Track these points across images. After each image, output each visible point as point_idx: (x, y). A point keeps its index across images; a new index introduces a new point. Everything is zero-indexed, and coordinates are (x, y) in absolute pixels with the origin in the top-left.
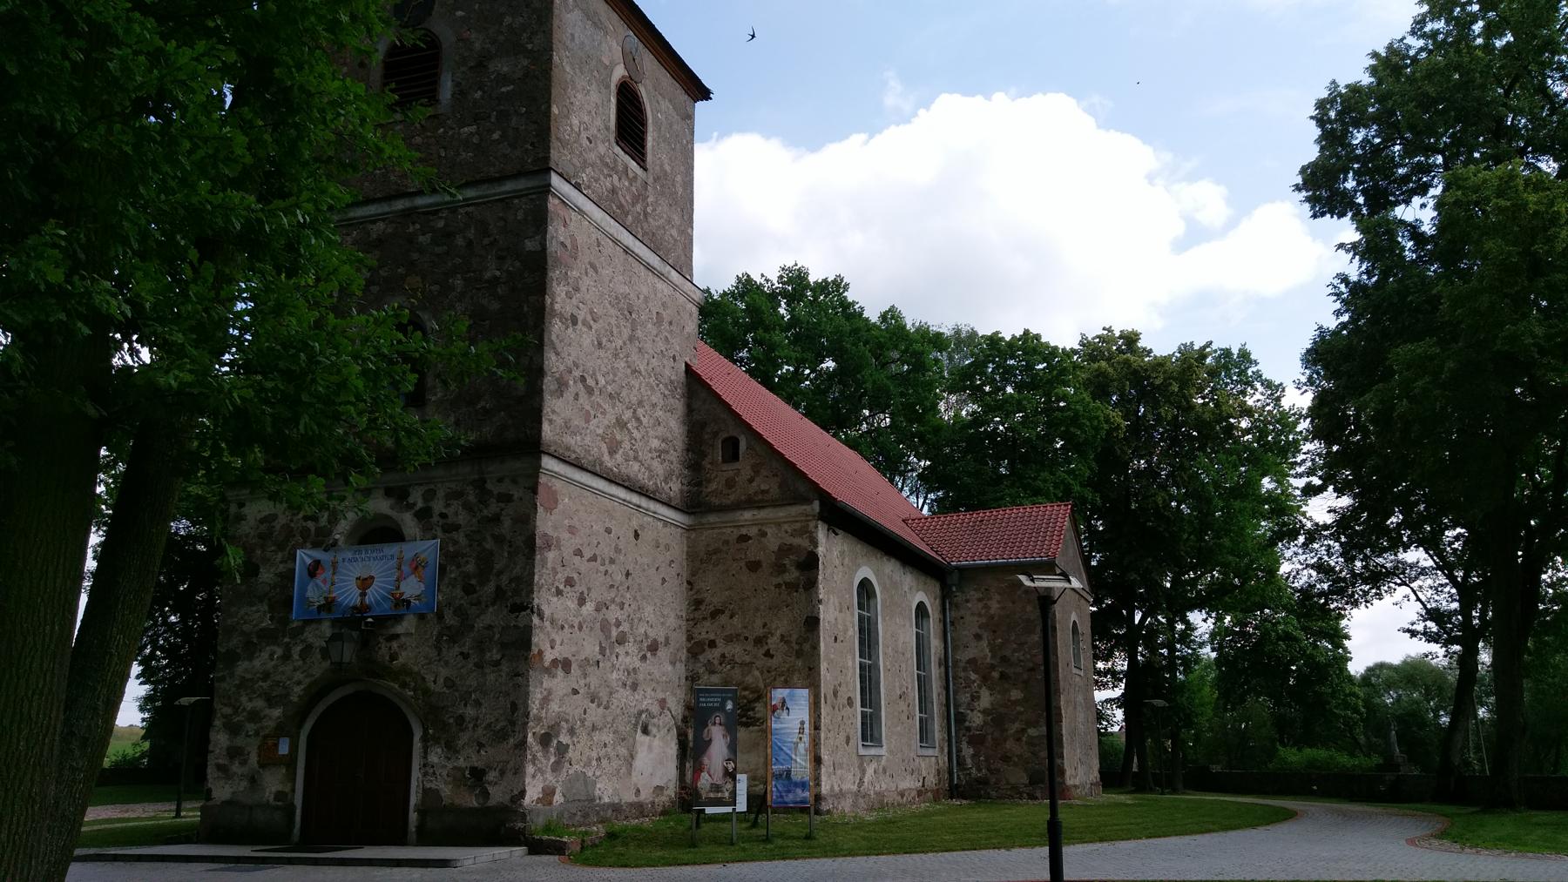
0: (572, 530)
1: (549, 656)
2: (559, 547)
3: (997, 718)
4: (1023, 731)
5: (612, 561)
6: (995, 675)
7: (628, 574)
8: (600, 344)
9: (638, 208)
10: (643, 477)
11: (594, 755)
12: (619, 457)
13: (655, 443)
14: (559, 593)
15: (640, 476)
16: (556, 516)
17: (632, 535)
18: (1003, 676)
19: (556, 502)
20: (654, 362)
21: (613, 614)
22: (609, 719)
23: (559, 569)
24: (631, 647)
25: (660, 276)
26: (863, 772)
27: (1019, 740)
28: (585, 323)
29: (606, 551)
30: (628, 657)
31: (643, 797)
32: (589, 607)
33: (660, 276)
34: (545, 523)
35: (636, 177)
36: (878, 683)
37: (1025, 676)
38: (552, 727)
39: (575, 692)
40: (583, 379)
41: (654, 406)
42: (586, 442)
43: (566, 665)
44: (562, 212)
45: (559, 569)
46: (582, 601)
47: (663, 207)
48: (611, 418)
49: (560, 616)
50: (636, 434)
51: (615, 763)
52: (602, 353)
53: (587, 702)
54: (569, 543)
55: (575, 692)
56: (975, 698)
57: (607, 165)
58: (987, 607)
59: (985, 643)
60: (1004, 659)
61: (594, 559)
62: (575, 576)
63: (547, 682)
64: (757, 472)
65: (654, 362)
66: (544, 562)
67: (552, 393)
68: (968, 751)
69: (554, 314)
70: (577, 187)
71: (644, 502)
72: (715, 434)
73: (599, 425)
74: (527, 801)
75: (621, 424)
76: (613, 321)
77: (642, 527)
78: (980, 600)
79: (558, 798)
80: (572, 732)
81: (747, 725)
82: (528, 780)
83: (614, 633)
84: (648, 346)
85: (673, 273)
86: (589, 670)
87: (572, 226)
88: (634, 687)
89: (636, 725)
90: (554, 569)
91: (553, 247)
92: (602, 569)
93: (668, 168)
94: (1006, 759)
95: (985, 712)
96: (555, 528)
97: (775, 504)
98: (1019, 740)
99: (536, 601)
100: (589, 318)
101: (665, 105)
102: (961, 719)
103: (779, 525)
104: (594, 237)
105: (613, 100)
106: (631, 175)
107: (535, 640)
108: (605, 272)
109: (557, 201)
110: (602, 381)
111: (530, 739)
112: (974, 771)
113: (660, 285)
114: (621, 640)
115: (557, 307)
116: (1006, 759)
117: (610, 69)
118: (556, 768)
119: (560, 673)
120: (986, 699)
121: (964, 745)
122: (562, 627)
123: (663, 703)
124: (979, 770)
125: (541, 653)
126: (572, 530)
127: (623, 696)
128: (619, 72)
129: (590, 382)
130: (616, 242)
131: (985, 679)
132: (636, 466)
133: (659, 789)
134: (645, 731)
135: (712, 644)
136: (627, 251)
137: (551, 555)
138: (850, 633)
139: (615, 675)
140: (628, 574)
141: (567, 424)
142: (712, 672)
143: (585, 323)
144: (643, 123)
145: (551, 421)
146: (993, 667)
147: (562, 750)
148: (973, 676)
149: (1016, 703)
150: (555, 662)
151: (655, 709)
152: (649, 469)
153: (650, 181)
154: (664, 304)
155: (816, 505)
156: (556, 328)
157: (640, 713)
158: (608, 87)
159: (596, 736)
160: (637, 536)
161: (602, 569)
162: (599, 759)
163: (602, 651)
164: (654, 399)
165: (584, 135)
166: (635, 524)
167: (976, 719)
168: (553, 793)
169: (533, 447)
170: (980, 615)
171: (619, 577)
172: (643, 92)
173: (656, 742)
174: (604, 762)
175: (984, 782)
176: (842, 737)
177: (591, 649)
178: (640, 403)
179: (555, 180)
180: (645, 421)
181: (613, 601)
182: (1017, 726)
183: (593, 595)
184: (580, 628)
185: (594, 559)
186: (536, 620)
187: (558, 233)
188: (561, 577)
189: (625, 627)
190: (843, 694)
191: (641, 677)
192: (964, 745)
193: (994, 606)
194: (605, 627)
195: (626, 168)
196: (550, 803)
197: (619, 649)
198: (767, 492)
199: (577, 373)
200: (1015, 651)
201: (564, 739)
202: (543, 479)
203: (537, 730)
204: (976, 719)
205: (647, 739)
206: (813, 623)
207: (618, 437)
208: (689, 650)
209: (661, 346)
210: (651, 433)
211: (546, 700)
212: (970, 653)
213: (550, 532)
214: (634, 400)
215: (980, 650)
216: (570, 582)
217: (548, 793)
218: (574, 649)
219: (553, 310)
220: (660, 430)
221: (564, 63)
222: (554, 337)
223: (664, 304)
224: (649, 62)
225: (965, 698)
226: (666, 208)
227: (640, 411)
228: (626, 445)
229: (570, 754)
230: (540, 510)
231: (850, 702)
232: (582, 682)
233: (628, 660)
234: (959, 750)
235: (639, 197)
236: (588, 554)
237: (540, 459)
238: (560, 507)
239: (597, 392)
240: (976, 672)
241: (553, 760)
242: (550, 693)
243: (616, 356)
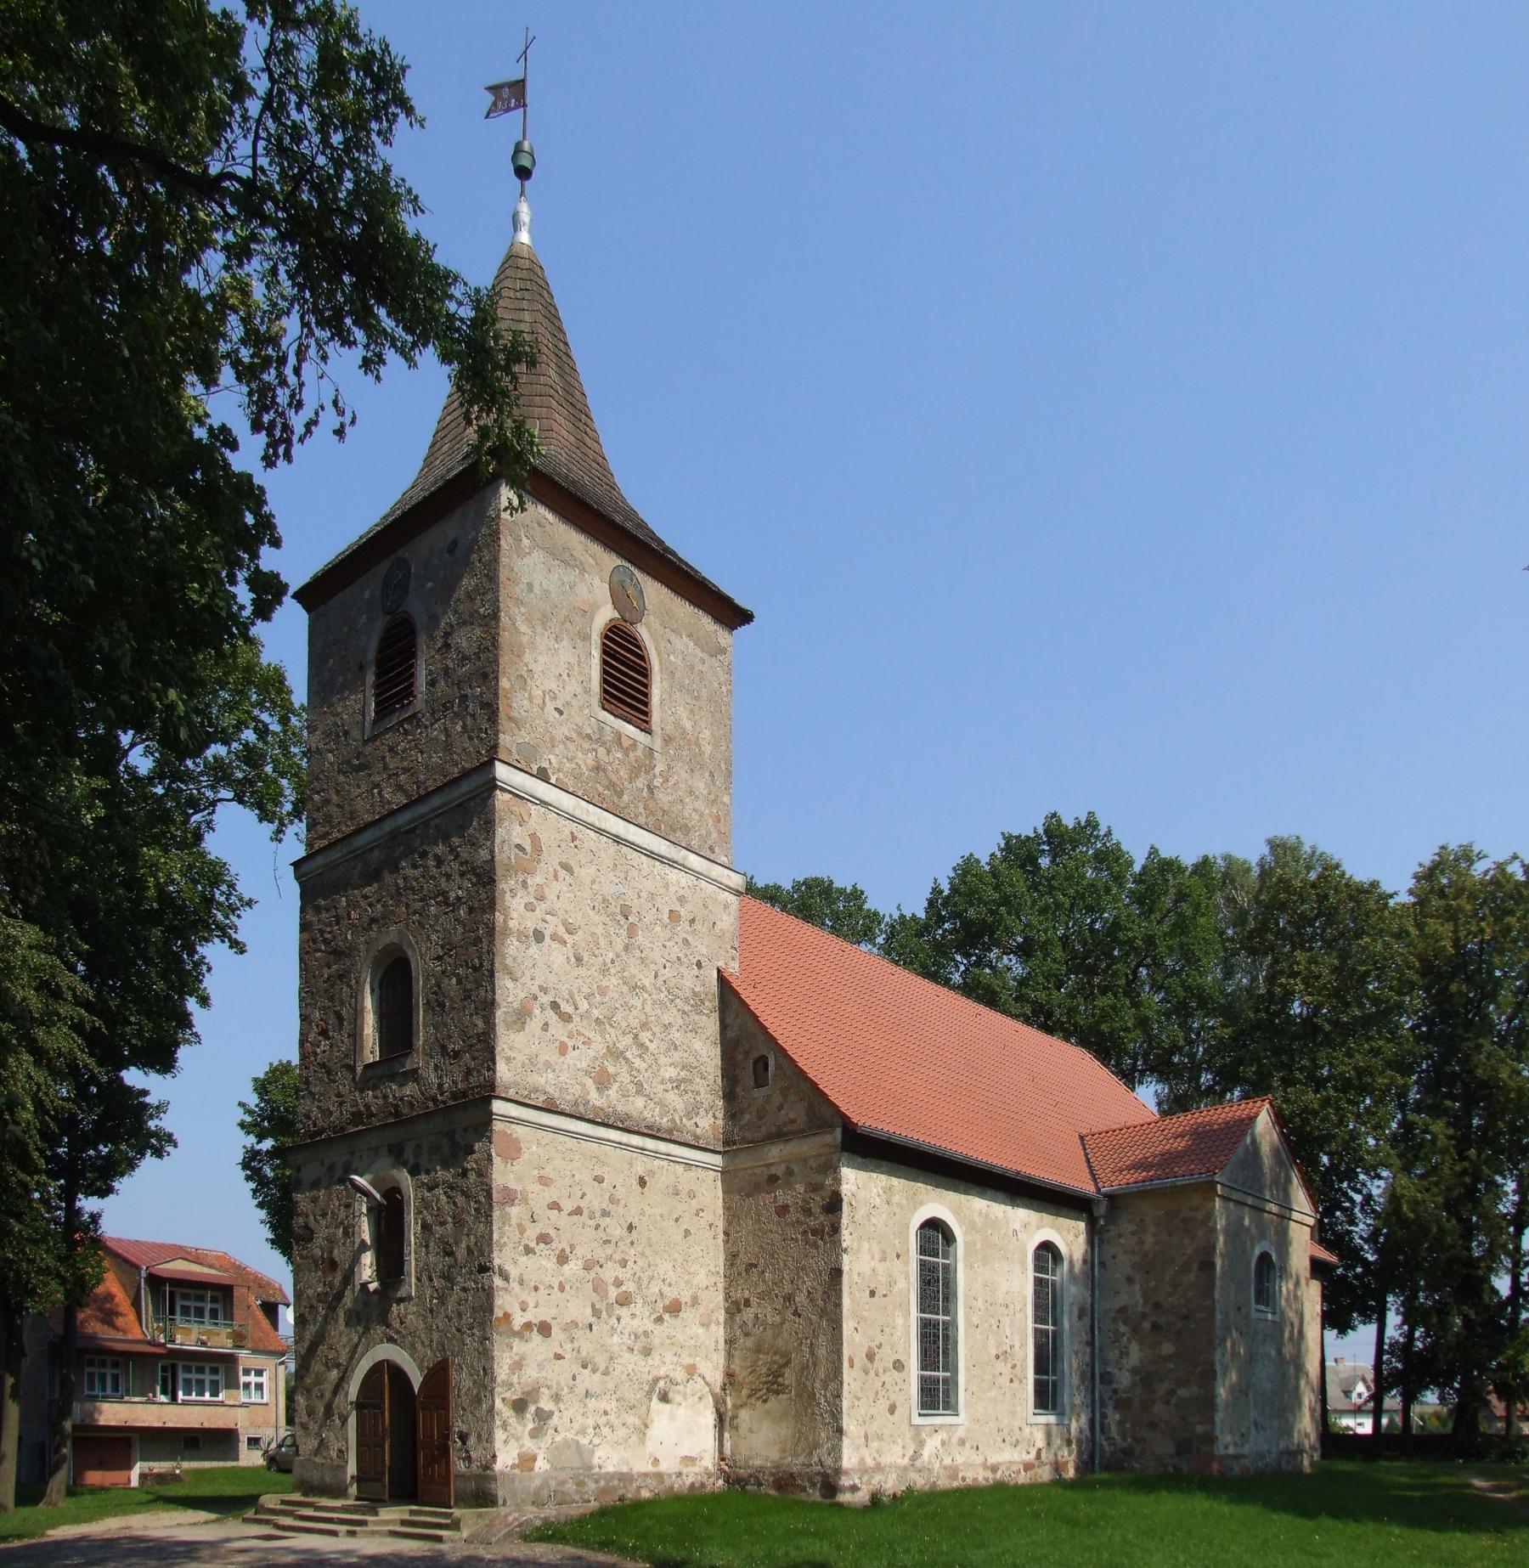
0: (544, 1181)
1: (518, 1320)
2: (525, 1201)
3: (1146, 1377)
4: (1172, 1392)
5: (605, 1214)
6: (1146, 1325)
7: (631, 1228)
8: (579, 959)
9: (640, 783)
10: (653, 1115)
11: (591, 1422)
12: (613, 1093)
13: (671, 1072)
14: (528, 1251)
15: (647, 1114)
16: (519, 1166)
17: (635, 1183)
18: (1155, 1327)
19: (519, 1150)
20: (667, 974)
21: (609, 1272)
22: (611, 1386)
23: (527, 1224)
24: (638, 1307)
25: (672, 863)
26: (922, 1444)
27: (1167, 1403)
28: (554, 937)
29: (595, 1200)
30: (637, 1319)
31: (663, 1467)
32: (573, 1267)
33: (672, 863)
34: (502, 1175)
35: (635, 744)
36: (956, 1343)
37: (1179, 1325)
38: (528, 1393)
39: (558, 1357)
40: (555, 1006)
41: (668, 1026)
42: (566, 1076)
43: (545, 1329)
44: (517, 807)
45: (527, 1224)
46: (562, 1259)
47: (681, 772)
48: (599, 1046)
49: (532, 1278)
50: (638, 1062)
51: (621, 1432)
52: (582, 971)
53: (577, 1369)
54: (539, 1197)
55: (558, 1357)
56: (1124, 1353)
57: (588, 736)
58: (1141, 1242)
59: (1137, 1287)
60: (1157, 1306)
61: (578, 1211)
62: (552, 1233)
63: (518, 1346)
64: (785, 1097)
65: (667, 974)
66: (506, 1219)
67: (508, 1027)
68: (1114, 1417)
69: (507, 932)
70: (542, 776)
71: (650, 1144)
72: (747, 1053)
73: (579, 1059)
74: (498, 1466)
75: (615, 1054)
76: (600, 930)
77: (652, 1173)
78: (1133, 1234)
79: (541, 1465)
80: (557, 1398)
81: (777, 1392)
82: (498, 1444)
83: (613, 1293)
84: (657, 955)
85: (692, 857)
86: (578, 1333)
87: (533, 824)
88: (647, 1352)
89: (649, 1393)
90: (520, 1226)
91: (504, 855)
92: (592, 1223)
93: (688, 725)
94: (1153, 1425)
95: (1134, 1371)
96: (519, 1179)
97: (802, 1134)
98: (1167, 1403)
99: (497, 1262)
100: (561, 931)
101: (682, 643)
102: (1107, 1379)
103: (805, 1160)
104: (567, 832)
105: (596, 654)
106: (626, 743)
107: (498, 1302)
108: (583, 872)
109: (507, 796)
110: (584, 1005)
111: (498, 1404)
112: (1118, 1439)
113: (674, 875)
114: (625, 1300)
115: (511, 924)
116: (1153, 1425)
117: (587, 613)
118: (535, 1434)
119: (536, 1337)
120: (1135, 1356)
121: (1110, 1411)
122: (536, 1289)
123: (691, 1370)
124: (1124, 1439)
125: (507, 1316)
126: (544, 1181)
127: (630, 1362)
128: (606, 614)
129: (566, 1008)
130: (600, 831)
131: (1135, 1330)
132: (640, 1102)
133: (689, 1460)
134: (664, 1398)
135: (747, 1303)
136: (618, 840)
137: (515, 1211)
138: (902, 1284)
139: (616, 1339)
140: (631, 1228)
141: (532, 1061)
142: (747, 1335)
143: (554, 937)
144: (645, 673)
145: (508, 1060)
146: (1144, 1316)
147: (543, 1416)
148: (1123, 1328)
149: (1168, 1358)
150: (528, 1326)
151: (680, 1375)
152: (661, 1103)
153: (657, 744)
154: (682, 900)
155: (838, 1133)
156: (511, 950)
157: (656, 1380)
158: (586, 638)
159: (592, 1404)
160: (642, 1182)
161: (592, 1223)
162: (597, 1427)
163: (596, 1313)
164: (666, 1018)
165: (550, 706)
166: (639, 1169)
167: (1124, 1379)
168: (534, 1459)
169: (489, 1091)
170: (1133, 1252)
171: (618, 1232)
172: (643, 632)
173: (681, 1411)
174: (605, 1431)
175: (1128, 1452)
176: (883, 1404)
177: (578, 1308)
178: (645, 1026)
179: (502, 771)
180: (652, 1046)
181: (610, 1258)
182: (1167, 1385)
183: (579, 1251)
184: (562, 1288)
185: (578, 1211)
186: (498, 1281)
187: (510, 834)
188: (532, 1232)
189: (629, 1286)
190: (886, 1357)
191: (656, 1341)
192: (1110, 1411)
193: (1149, 1240)
194: (599, 1287)
195: (618, 736)
196: (532, 1469)
197: (624, 1312)
198: (793, 1121)
199: (545, 999)
200: (1170, 1294)
201: (546, 1404)
202: (498, 1126)
203: (507, 1395)
204: (1124, 1379)
205: (663, 1406)
206: (837, 1273)
207: (611, 1070)
208: (727, 1311)
209: (675, 951)
210: (663, 1060)
211: (518, 1366)
212: (1122, 1300)
213: (512, 1185)
214: (635, 1023)
215: (1132, 1297)
216: (544, 1239)
217: (527, 1461)
218: (553, 1312)
219: (506, 928)
220: (677, 1056)
221: (516, 622)
222: (509, 961)
223: (682, 900)
224: (654, 593)
225: (1113, 1354)
226: (684, 775)
227: (645, 1036)
228: (625, 1077)
229: (554, 1421)
230: (497, 1160)
231: (899, 1365)
232: (568, 1347)
233: (636, 1322)
234: (1104, 1416)
235: (643, 767)
236: (568, 1206)
237: (490, 1104)
238: (525, 1156)
239: (576, 1019)
240: (1125, 1323)
241: (531, 1426)
242: (523, 1358)
243: (605, 971)
